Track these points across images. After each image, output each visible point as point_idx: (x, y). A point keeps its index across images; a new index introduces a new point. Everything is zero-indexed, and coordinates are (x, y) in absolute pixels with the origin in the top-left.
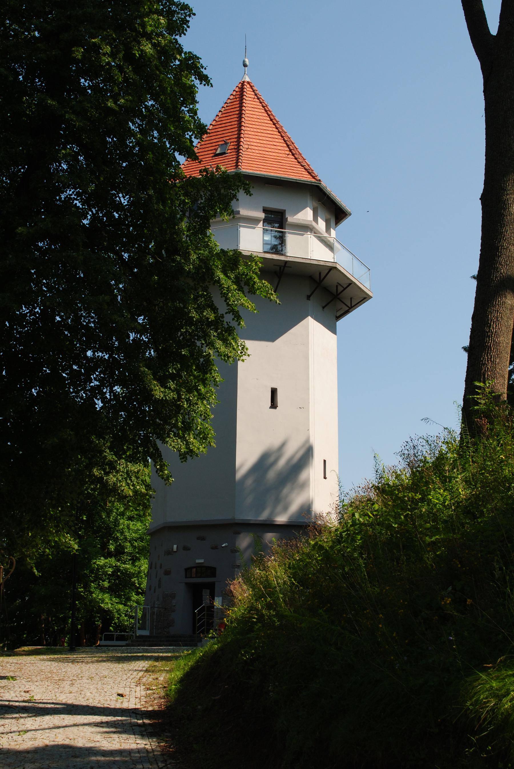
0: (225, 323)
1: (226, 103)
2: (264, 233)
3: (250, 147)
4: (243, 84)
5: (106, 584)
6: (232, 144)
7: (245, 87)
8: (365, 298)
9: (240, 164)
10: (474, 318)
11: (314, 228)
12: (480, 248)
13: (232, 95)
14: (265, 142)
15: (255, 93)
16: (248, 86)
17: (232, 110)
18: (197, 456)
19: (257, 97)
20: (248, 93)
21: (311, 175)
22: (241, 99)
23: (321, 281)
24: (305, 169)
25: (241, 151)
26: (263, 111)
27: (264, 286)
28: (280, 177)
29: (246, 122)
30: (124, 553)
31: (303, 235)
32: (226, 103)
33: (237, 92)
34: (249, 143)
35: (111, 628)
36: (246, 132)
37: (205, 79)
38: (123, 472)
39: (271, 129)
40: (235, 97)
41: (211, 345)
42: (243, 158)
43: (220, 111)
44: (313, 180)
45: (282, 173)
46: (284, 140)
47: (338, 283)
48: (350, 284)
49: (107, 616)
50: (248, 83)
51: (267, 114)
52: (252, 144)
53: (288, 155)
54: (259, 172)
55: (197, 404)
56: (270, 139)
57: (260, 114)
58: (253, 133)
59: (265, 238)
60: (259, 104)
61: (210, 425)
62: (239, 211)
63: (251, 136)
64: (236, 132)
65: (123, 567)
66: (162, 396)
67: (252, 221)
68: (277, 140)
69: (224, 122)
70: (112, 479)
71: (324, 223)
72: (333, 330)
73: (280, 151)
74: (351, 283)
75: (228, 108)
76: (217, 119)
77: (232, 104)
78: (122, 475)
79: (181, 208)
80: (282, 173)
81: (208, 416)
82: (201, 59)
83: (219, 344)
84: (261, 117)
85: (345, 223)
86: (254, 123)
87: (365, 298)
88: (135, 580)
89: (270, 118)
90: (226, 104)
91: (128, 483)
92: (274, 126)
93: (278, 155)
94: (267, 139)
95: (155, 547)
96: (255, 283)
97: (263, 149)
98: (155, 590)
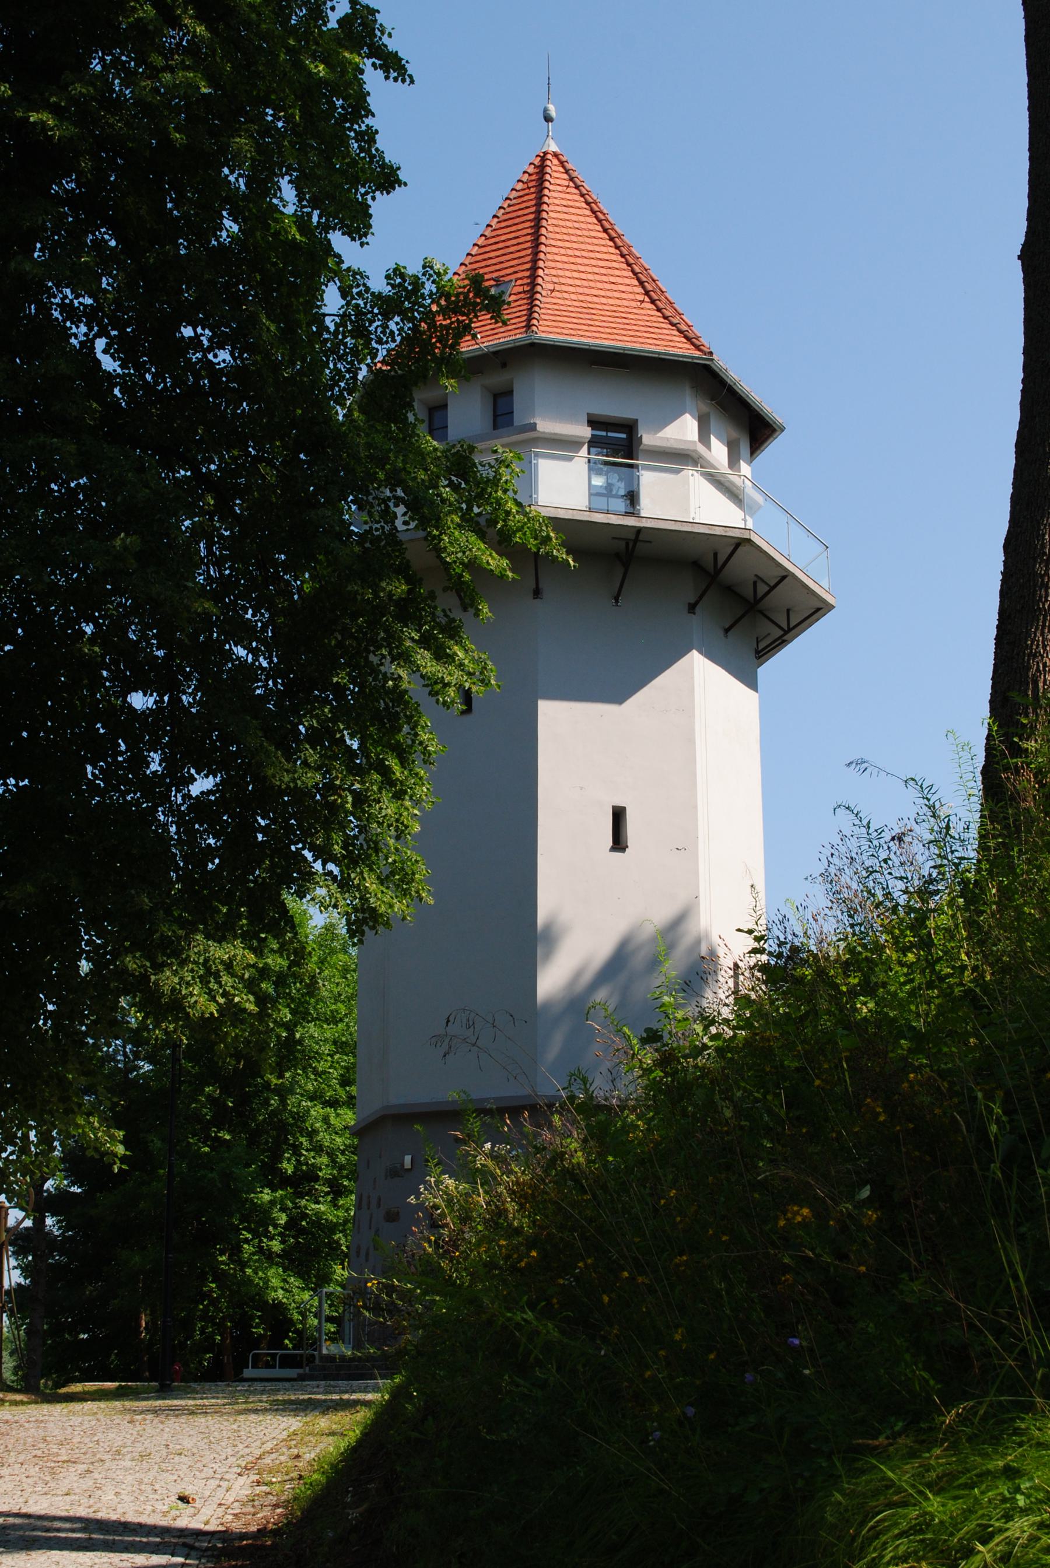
0: (439, 612)
1: (507, 199)
2: (590, 469)
3: (558, 287)
4: (543, 158)
5: (276, 1246)
6: (519, 282)
7: (548, 163)
8: (819, 609)
9: (535, 322)
10: (1009, 546)
11: (700, 457)
12: (1022, 376)
13: (519, 181)
14: (590, 277)
15: (569, 175)
16: (555, 162)
17: (520, 213)
18: (387, 924)
19: (574, 183)
20: (555, 174)
21: (693, 344)
22: (539, 188)
23: (718, 570)
24: (679, 331)
25: (538, 296)
26: (588, 213)
27: (529, 520)
28: (624, 349)
29: (549, 235)
30: (317, 1179)
31: (678, 471)
32: (507, 199)
33: (530, 175)
34: (555, 279)
35: (287, 1342)
36: (549, 256)
37: (393, 65)
38: (195, 962)
39: (604, 249)
40: (525, 186)
41: (404, 658)
42: (542, 311)
43: (495, 216)
44: (697, 354)
45: (628, 339)
46: (633, 271)
47: (756, 576)
48: (784, 578)
49: (277, 1317)
50: (556, 155)
51: (597, 217)
52: (563, 280)
53: (642, 302)
54: (575, 339)
55: (379, 802)
56: (603, 271)
57: (582, 219)
58: (565, 259)
59: (594, 483)
60: (578, 198)
61: (413, 849)
62: (535, 424)
63: (559, 265)
64: (529, 258)
65: (313, 1210)
66: (286, 779)
67: (566, 445)
68: (617, 273)
69: (503, 238)
70: (168, 980)
71: (726, 449)
72: (751, 683)
73: (624, 296)
74: (785, 576)
75: (512, 209)
76: (488, 233)
77: (519, 200)
78: (192, 971)
79: (348, 363)
80: (628, 339)
81: (407, 827)
82: (378, 12)
83: (424, 659)
84: (583, 226)
85: (773, 449)
86: (566, 237)
87: (819, 609)
88: (340, 1238)
89: (602, 226)
90: (508, 202)
91: (211, 990)
92: (611, 243)
93: (619, 302)
94: (596, 270)
95: (368, 1162)
96: (508, 513)
97: (587, 291)
98: (367, 1254)
